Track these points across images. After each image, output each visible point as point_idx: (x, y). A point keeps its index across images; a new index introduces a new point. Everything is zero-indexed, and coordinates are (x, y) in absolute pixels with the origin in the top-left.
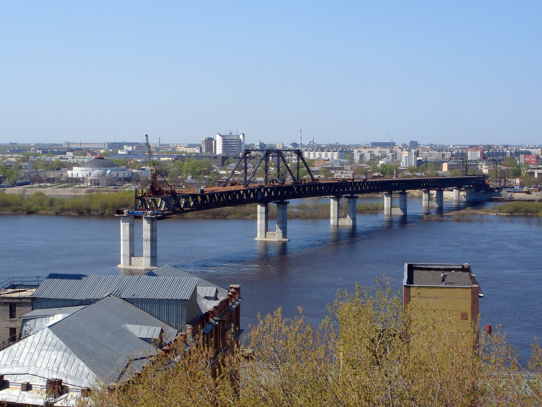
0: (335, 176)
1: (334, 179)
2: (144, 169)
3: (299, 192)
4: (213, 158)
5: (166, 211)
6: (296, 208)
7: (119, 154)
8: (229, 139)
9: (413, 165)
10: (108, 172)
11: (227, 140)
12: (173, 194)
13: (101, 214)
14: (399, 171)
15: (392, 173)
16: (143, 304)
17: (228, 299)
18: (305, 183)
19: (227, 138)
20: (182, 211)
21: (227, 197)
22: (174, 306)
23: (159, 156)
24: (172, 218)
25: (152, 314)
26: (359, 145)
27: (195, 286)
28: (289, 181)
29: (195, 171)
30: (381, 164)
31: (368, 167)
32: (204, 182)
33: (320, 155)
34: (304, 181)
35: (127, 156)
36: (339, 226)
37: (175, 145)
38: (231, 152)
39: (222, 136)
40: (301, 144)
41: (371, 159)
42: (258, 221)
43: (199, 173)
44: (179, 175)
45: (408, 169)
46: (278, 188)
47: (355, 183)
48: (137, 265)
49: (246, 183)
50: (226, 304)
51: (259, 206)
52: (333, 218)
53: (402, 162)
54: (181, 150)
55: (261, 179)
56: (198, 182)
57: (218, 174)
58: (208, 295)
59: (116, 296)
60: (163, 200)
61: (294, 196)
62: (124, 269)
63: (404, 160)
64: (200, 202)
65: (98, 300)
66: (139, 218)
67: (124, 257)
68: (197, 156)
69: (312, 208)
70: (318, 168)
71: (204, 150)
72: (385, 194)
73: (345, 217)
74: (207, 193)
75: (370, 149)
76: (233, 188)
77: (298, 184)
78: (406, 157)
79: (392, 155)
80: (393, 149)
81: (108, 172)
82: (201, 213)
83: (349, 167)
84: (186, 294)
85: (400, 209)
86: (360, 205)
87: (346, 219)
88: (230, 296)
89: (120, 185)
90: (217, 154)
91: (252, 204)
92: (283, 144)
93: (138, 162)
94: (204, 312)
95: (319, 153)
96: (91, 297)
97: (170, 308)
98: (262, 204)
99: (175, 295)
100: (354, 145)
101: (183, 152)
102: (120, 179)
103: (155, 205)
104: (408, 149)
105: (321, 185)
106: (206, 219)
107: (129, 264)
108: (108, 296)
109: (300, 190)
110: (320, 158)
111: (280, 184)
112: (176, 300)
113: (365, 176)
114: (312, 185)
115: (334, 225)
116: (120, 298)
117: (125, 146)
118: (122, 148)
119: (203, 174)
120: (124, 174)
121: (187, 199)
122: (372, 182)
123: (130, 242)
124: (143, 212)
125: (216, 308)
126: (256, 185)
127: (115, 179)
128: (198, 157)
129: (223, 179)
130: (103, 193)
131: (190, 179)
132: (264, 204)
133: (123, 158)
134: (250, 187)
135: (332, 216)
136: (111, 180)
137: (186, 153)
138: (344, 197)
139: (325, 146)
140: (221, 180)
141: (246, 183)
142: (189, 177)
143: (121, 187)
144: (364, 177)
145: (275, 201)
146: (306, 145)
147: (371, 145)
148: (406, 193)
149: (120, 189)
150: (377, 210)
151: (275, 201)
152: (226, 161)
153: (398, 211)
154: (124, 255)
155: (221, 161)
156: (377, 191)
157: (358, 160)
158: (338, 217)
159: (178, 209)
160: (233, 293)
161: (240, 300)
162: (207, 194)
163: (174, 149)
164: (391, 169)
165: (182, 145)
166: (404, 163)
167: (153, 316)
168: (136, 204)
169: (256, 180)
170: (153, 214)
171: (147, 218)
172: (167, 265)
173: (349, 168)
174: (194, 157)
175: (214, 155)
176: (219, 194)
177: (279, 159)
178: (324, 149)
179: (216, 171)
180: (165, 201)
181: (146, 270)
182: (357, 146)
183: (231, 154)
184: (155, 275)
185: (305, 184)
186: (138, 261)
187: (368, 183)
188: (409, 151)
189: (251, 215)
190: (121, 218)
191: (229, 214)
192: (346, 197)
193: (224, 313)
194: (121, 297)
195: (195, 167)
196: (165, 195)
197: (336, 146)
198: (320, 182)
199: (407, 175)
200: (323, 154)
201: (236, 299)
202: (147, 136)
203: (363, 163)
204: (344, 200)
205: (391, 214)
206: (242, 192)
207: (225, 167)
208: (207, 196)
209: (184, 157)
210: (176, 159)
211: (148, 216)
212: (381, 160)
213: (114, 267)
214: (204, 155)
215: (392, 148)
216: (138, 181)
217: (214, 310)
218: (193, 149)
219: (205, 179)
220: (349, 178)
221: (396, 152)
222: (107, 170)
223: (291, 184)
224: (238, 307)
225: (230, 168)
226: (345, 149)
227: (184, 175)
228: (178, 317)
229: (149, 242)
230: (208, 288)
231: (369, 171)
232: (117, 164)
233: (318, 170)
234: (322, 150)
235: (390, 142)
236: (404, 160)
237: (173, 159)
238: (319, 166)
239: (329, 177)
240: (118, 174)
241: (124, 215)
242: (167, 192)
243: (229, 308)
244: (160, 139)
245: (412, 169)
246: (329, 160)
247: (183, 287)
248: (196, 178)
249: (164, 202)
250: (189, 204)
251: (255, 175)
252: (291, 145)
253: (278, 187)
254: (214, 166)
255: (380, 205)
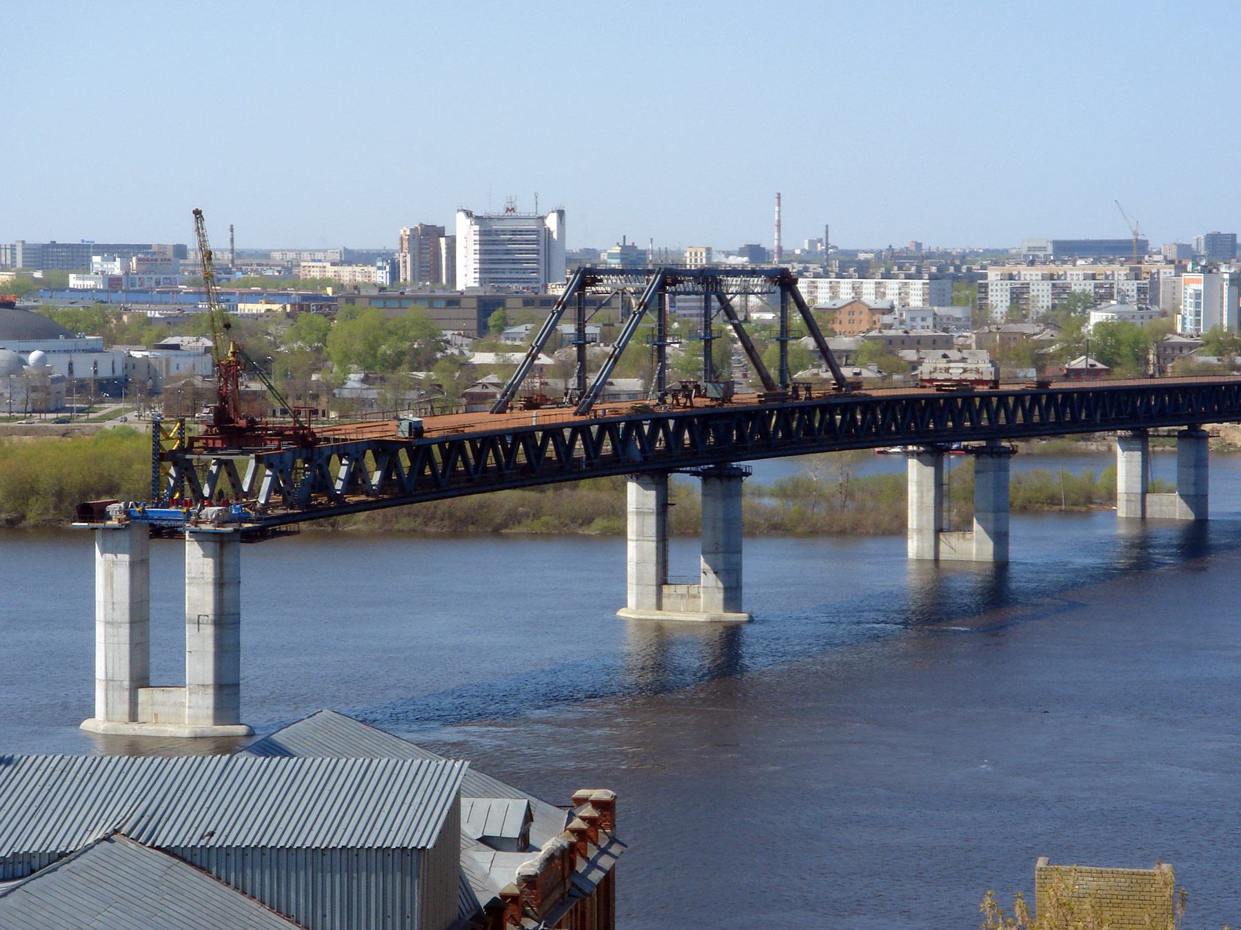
0: (925, 371)
1: (922, 380)
2: (176, 347)
3: (788, 433)
4: (443, 304)
5: (275, 506)
6: (772, 495)
7: (73, 290)
8: (504, 232)
9: (1225, 322)
10: (34, 356)
11: (497, 232)
12: (306, 442)
13: (7, 520)
14: (1169, 351)
15: (1141, 359)
16: (249, 871)
17: (572, 845)
18: (810, 398)
19: (496, 226)
20: (343, 508)
21: (480, 454)
22: (373, 876)
23: (231, 298)
24: (298, 532)
25: (284, 910)
26: (1006, 251)
27: (454, 793)
28: (747, 393)
29: (375, 356)
30: (1098, 325)
31: (1047, 335)
32: (412, 395)
33: (856, 290)
34: (808, 389)
35: (103, 297)
36: (942, 565)
37: (291, 256)
38: (512, 280)
39: (479, 220)
40: (780, 249)
41: (1054, 306)
42: (632, 547)
43: (395, 363)
44: (316, 370)
45: (1208, 343)
46: (701, 422)
47: (1003, 397)
48: (160, 719)
49: (586, 398)
50: (567, 865)
51: (632, 488)
52: (920, 531)
53: (1179, 317)
54: (316, 274)
55: (628, 383)
56: (389, 396)
57: (464, 365)
58: (492, 831)
59: (136, 839)
60: (262, 466)
61: (769, 449)
62: (106, 736)
63: (1188, 307)
64: (406, 471)
65: (60, 857)
66: (168, 533)
67: (106, 690)
68: (384, 297)
69: (833, 496)
70: (852, 339)
71: (406, 274)
72: (1120, 437)
73: (964, 526)
74: (435, 435)
75: (1052, 266)
76: (533, 418)
77: (784, 401)
78: (1198, 295)
79: (1139, 289)
80: (1144, 267)
81: (34, 356)
82: (404, 517)
83: (971, 337)
84: (421, 828)
85: (1182, 496)
86: (1020, 483)
87: (968, 536)
88: (579, 833)
89: (80, 410)
90: (460, 286)
91: (604, 481)
92: (709, 250)
93: (150, 321)
94: (484, 899)
95: (853, 284)
96: (32, 844)
97: (355, 882)
98: (647, 479)
99: (375, 832)
100: (986, 251)
101: (326, 282)
102: (81, 387)
103: (233, 485)
104: (1203, 263)
105: (869, 404)
106: (425, 535)
107: (126, 718)
108: (104, 839)
109: (789, 424)
110: (857, 301)
111: (712, 399)
112: (380, 854)
113: (1034, 370)
114: (837, 405)
115: (920, 561)
116: (152, 847)
117: (96, 259)
118: (83, 267)
119: (406, 366)
120: (95, 363)
121: (357, 460)
122: (1067, 394)
123: (132, 628)
124: (185, 510)
125: (528, 881)
126: (625, 406)
127: (63, 386)
128: (385, 299)
129: (484, 386)
130: (15, 438)
131: (357, 385)
132: (653, 477)
133: (91, 304)
134: (600, 413)
135: (912, 522)
136: (46, 389)
137: (339, 287)
138: (957, 449)
139: (871, 256)
140: (477, 390)
141: (586, 398)
142: (354, 379)
143: (84, 417)
144: (1032, 373)
145: (693, 469)
146: (798, 252)
147: (1050, 250)
148: (1205, 436)
149: (81, 423)
150: (1089, 500)
151: (693, 469)
152: (496, 314)
153: (1173, 503)
154: (107, 681)
155: (475, 316)
156: (1086, 428)
157: (1004, 310)
158: (939, 531)
159: (324, 500)
160: (590, 821)
161: (615, 850)
162: (434, 441)
163: (288, 269)
164: (1137, 342)
165: (319, 256)
166: (1190, 318)
167: (288, 917)
168: (157, 482)
169: (612, 388)
170: (226, 518)
171: (200, 537)
172: (326, 712)
173: (972, 341)
174: (372, 298)
175: (447, 294)
176: (447, 445)
177: (707, 308)
178: (868, 268)
179: (456, 352)
180: (270, 466)
181: (195, 738)
182: (998, 258)
183: (514, 287)
184: (283, 752)
185: (809, 402)
186: (163, 704)
187: (1052, 395)
188: (1210, 272)
189: (599, 524)
190: (98, 534)
191: (514, 518)
192: (967, 451)
193: (561, 904)
194: (157, 844)
195: (376, 340)
196: (272, 445)
197: (914, 258)
198: (868, 392)
199: (1204, 363)
200: (868, 286)
201: (599, 848)
202: (197, 213)
203: (1023, 322)
204: (959, 465)
205: (1143, 517)
206: (567, 433)
207: (490, 339)
208: (435, 448)
209: (328, 299)
210: (301, 308)
211: (204, 527)
212: (1095, 306)
213: (73, 729)
214: (408, 292)
215: (1140, 263)
216: (153, 392)
217: (522, 892)
218: (366, 269)
219: (418, 384)
220: (977, 377)
221: (1152, 275)
222: (29, 352)
223: (757, 400)
224: (609, 878)
225: (509, 342)
226: (952, 269)
227: (335, 369)
228: (389, 921)
229: (209, 631)
230: (496, 802)
231: (1051, 350)
232: (69, 326)
233: (853, 347)
234: (864, 271)
235: (1130, 236)
236: (1188, 307)
237: (288, 308)
238: (852, 334)
239: (896, 377)
240: (71, 364)
241: (109, 523)
242: (280, 433)
243: (578, 882)
244: (232, 230)
245: (1220, 343)
246: (891, 310)
247: (408, 801)
248: (382, 379)
249: (268, 472)
250: (364, 481)
251: (617, 369)
252: (741, 253)
253: (708, 411)
254: (449, 334)
255: (1101, 481)
